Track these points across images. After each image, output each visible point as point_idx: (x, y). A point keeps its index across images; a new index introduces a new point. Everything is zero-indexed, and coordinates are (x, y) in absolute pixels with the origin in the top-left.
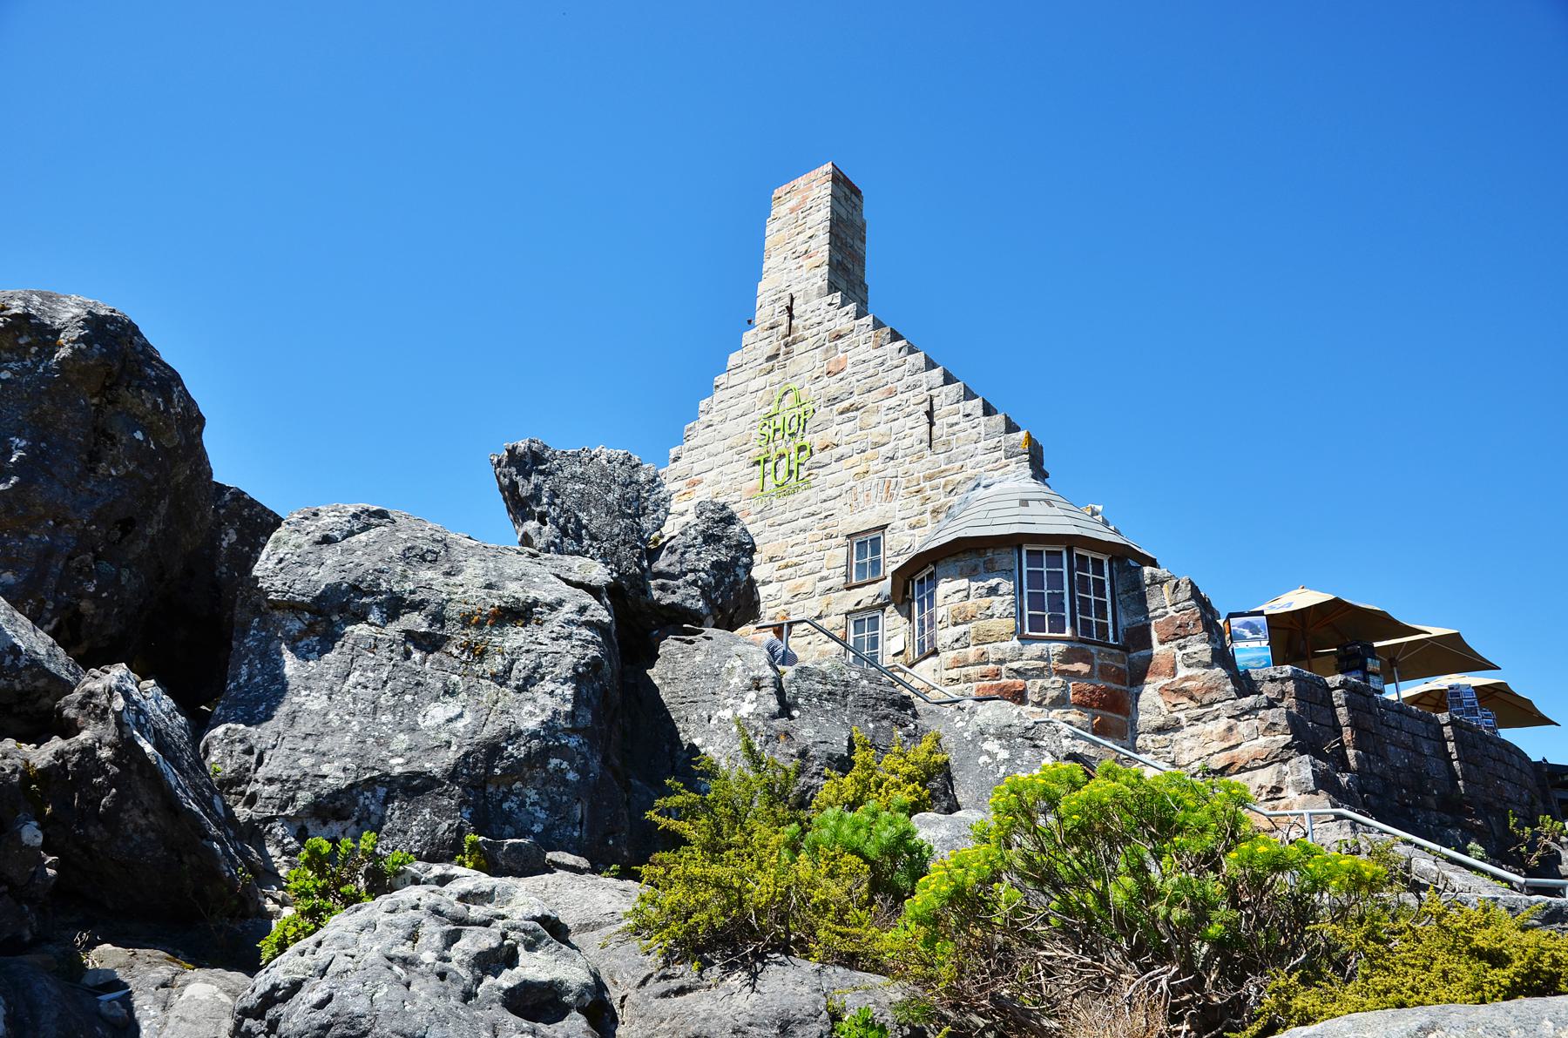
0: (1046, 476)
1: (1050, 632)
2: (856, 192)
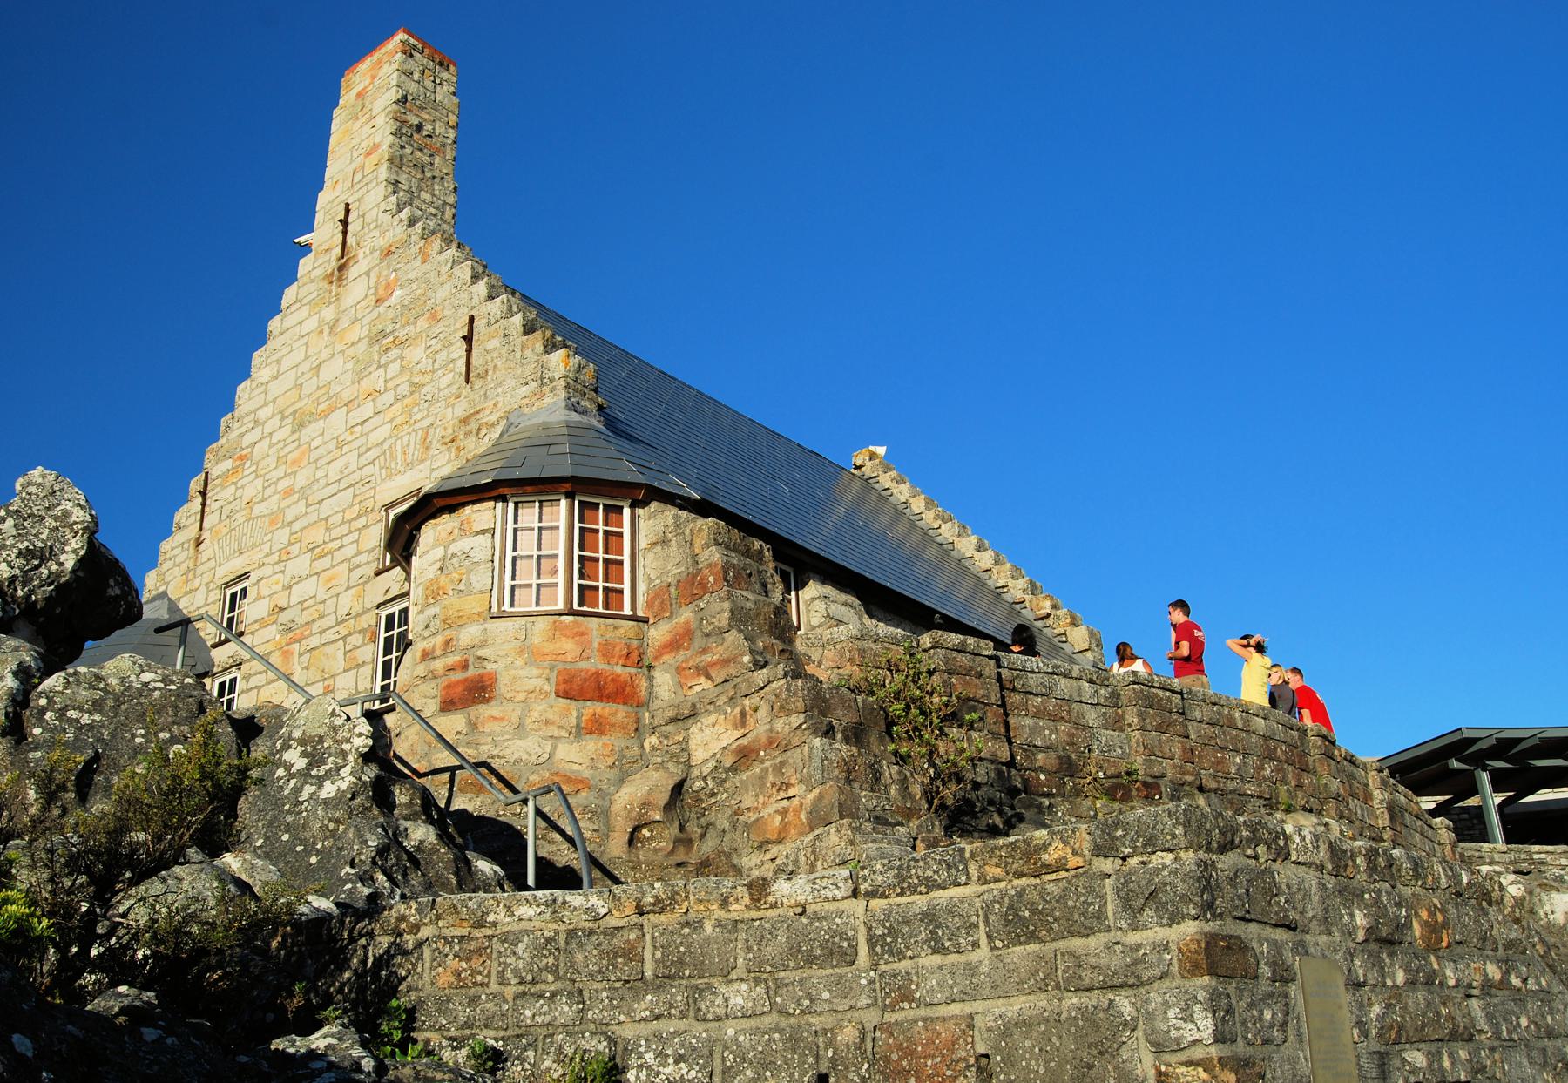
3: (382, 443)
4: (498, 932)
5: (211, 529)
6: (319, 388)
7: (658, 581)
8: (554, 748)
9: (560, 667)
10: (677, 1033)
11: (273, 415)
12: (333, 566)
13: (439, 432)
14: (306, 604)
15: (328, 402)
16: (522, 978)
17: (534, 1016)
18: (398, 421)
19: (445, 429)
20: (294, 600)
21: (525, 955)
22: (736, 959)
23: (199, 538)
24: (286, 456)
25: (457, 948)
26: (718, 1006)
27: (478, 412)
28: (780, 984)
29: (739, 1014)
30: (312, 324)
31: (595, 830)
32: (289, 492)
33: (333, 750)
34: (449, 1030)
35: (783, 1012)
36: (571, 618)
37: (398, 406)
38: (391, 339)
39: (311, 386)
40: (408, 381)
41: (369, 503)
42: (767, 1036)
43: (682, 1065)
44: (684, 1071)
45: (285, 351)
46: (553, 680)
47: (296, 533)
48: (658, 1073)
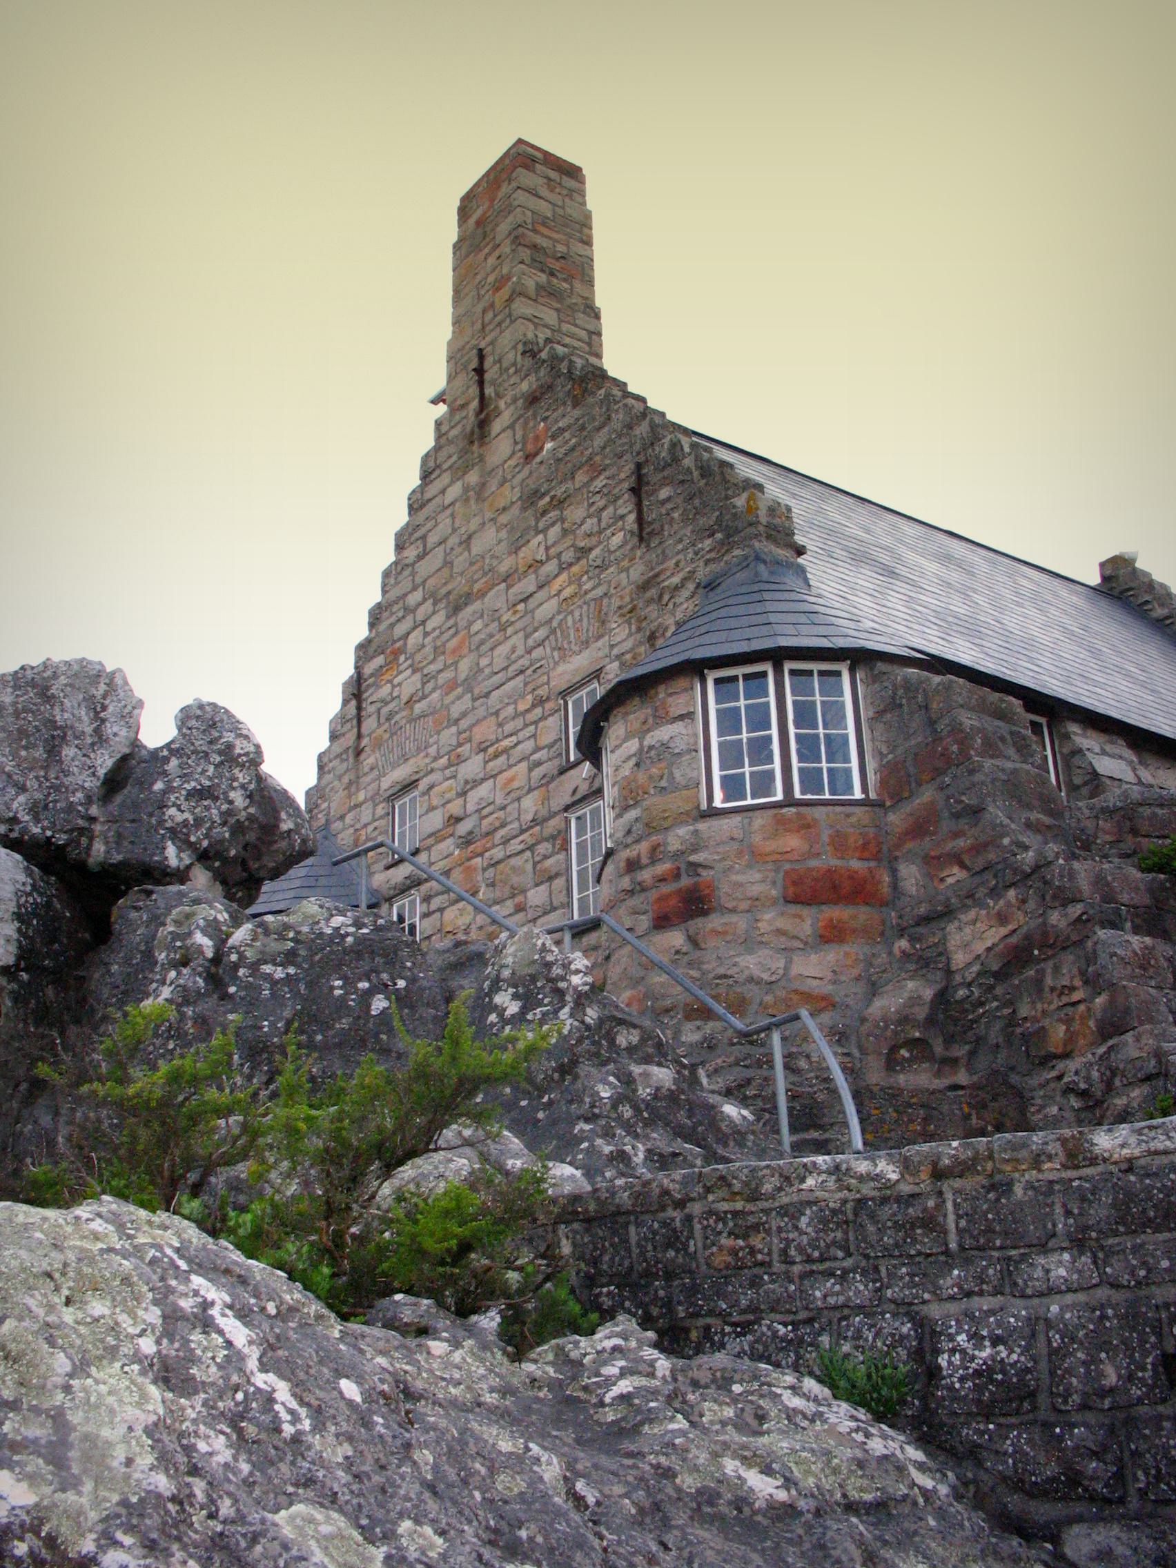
1: (753, 798)
3: (551, 619)
4: (777, 1204)
5: (370, 735)
6: (472, 564)
7: (890, 756)
8: (789, 962)
9: (787, 866)
10: (992, 1312)
11: (425, 600)
12: (510, 766)
13: (616, 602)
14: (485, 812)
15: (484, 580)
16: (809, 1256)
17: (825, 1296)
18: (567, 593)
19: (622, 597)
20: (471, 808)
21: (810, 1230)
22: (1054, 1225)
23: (359, 744)
24: (444, 645)
25: (731, 1224)
26: (1037, 1279)
27: (656, 576)
28: (1110, 1252)
29: (1063, 1287)
30: (455, 491)
31: (845, 1054)
32: (452, 685)
33: (547, 990)
34: (730, 1314)
35: (1116, 1286)
36: (793, 810)
37: (564, 577)
38: (547, 499)
39: (460, 561)
40: (572, 546)
41: (543, 692)
42: (1098, 1313)
43: (1001, 1348)
44: (1004, 1355)
45: (429, 525)
46: (780, 883)
47: (465, 731)
48: (973, 1358)
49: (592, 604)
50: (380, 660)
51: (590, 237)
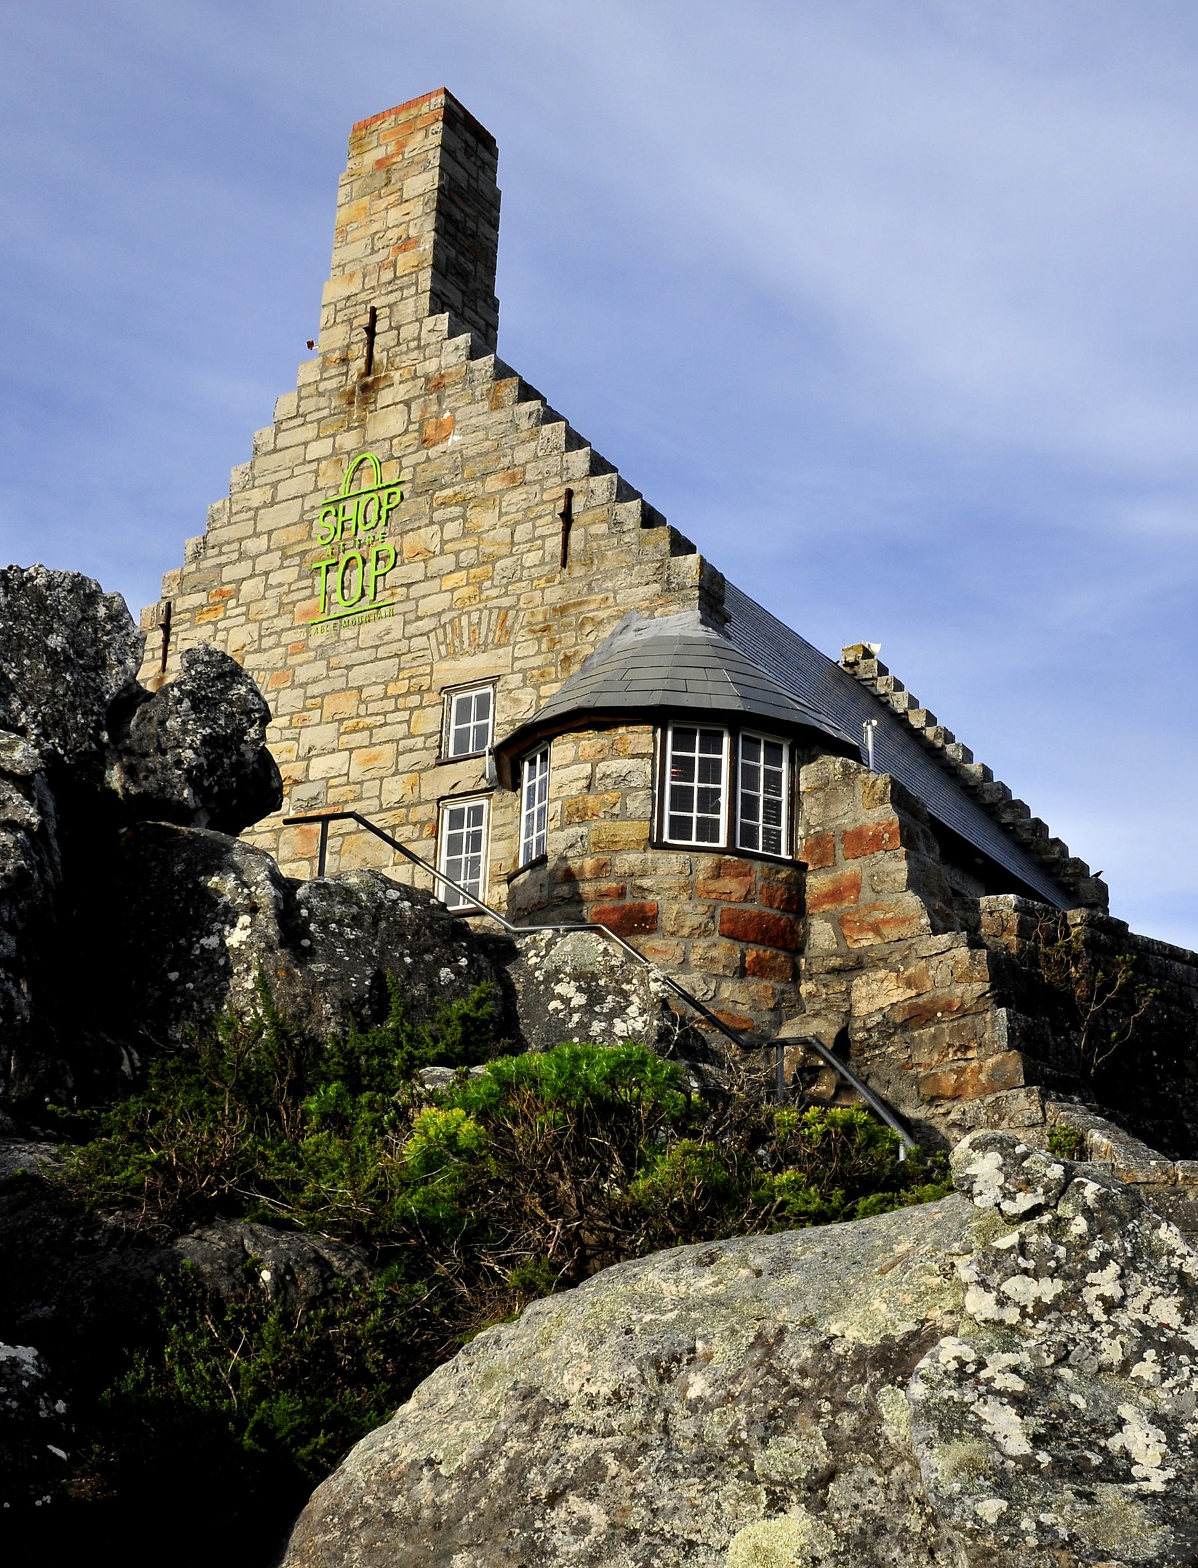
0: (727, 620)
1: (698, 840)
2: (487, 141)
13: (524, 617)
14: (333, 782)
30: (321, 448)
49: (496, 612)
50: (199, 598)
51: (497, 219)
